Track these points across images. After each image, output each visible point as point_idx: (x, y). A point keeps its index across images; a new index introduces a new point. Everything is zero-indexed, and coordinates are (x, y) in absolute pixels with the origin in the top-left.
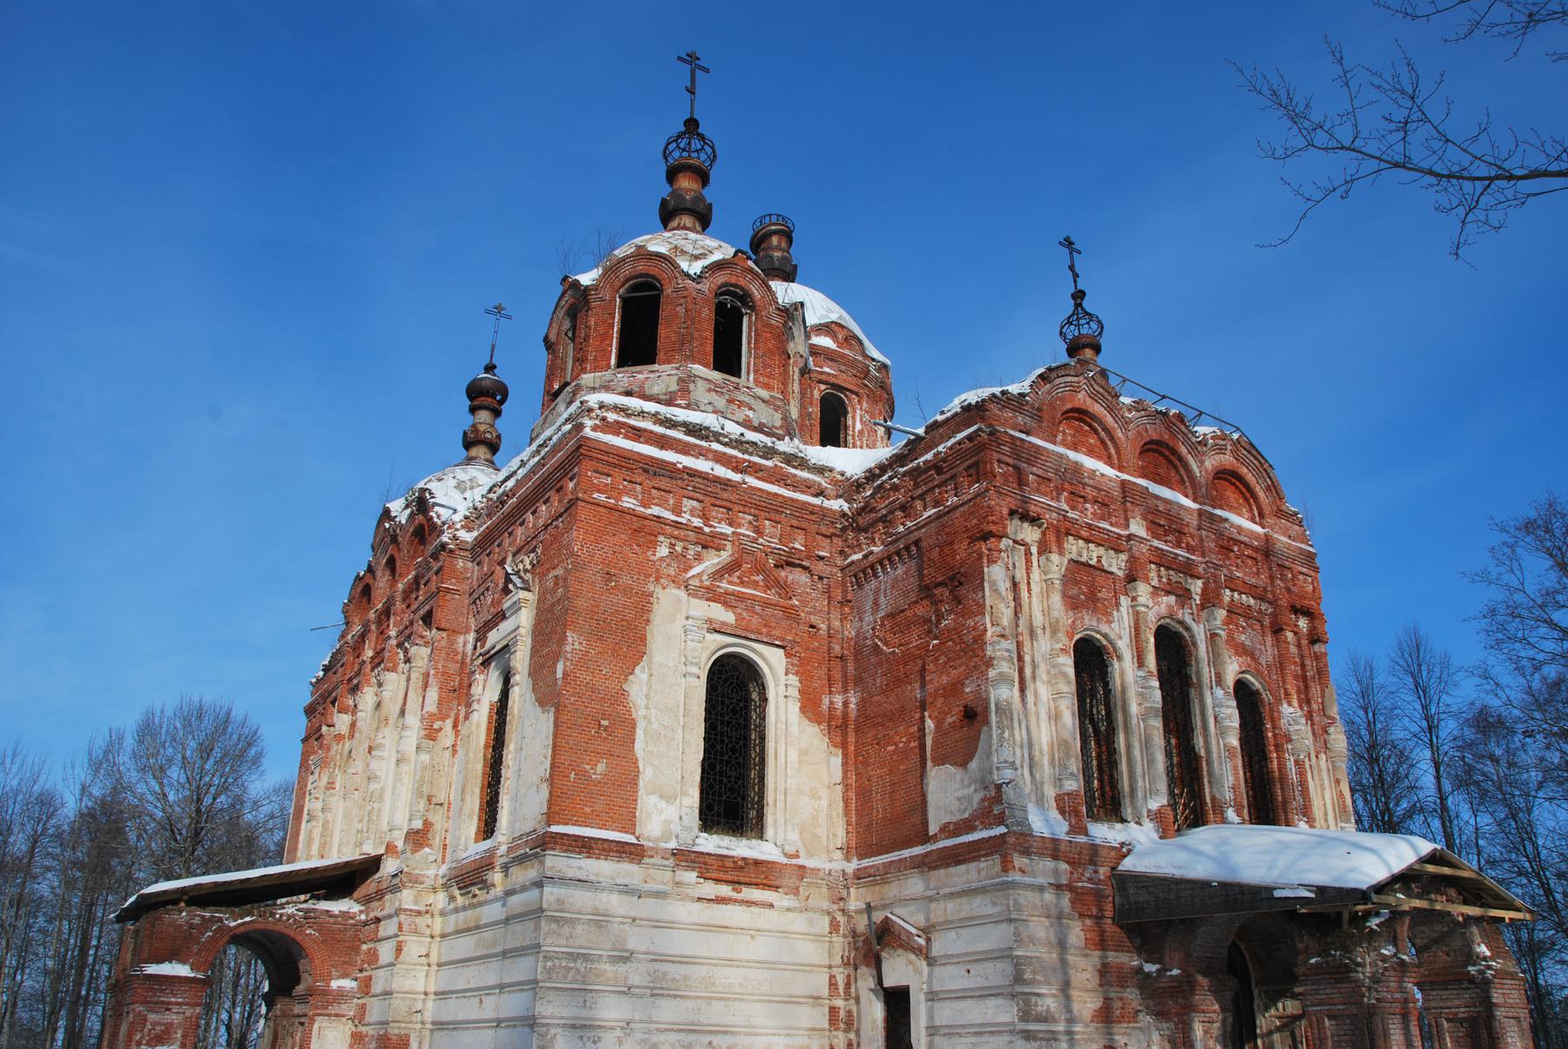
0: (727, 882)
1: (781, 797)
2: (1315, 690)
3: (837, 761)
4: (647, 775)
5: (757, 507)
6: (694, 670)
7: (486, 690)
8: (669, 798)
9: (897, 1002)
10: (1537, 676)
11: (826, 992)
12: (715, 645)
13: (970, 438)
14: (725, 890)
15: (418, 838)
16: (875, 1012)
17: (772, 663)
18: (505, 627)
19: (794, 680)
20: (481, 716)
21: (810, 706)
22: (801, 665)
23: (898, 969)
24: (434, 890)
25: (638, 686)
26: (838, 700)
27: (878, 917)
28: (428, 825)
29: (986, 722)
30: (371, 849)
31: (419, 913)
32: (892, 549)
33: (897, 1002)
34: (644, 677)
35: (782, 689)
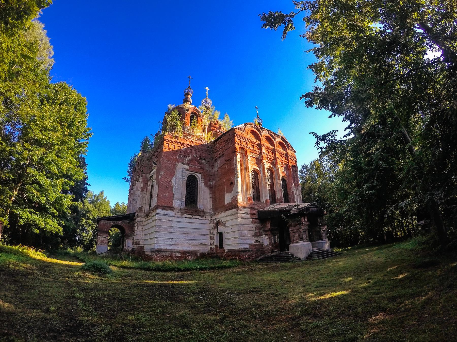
0: (190, 215)
1: (200, 200)
2: (296, 179)
3: (209, 191)
4: (175, 196)
5: (196, 149)
6: (184, 178)
7: (150, 183)
8: (179, 200)
9: (221, 234)
10: (360, 335)
11: (209, 233)
12: (188, 173)
13: (324, 294)
14: (190, 216)
15: (141, 209)
16: (216, 237)
17: (199, 176)
18: (153, 172)
19: (203, 180)
20: (150, 187)
21: (206, 184)
22: (204, 177)
23: (221, 228)
24: (143, 218)
25: (173, 180)
26: (211, 183)
27: (217, 220)
28: (142, 207)
29: (234, 184)
30: (134, 212)
31: (141, 222)
32: (220, 155)
33: (221, 234)
34: (175, 179)
35: (200, 181)
